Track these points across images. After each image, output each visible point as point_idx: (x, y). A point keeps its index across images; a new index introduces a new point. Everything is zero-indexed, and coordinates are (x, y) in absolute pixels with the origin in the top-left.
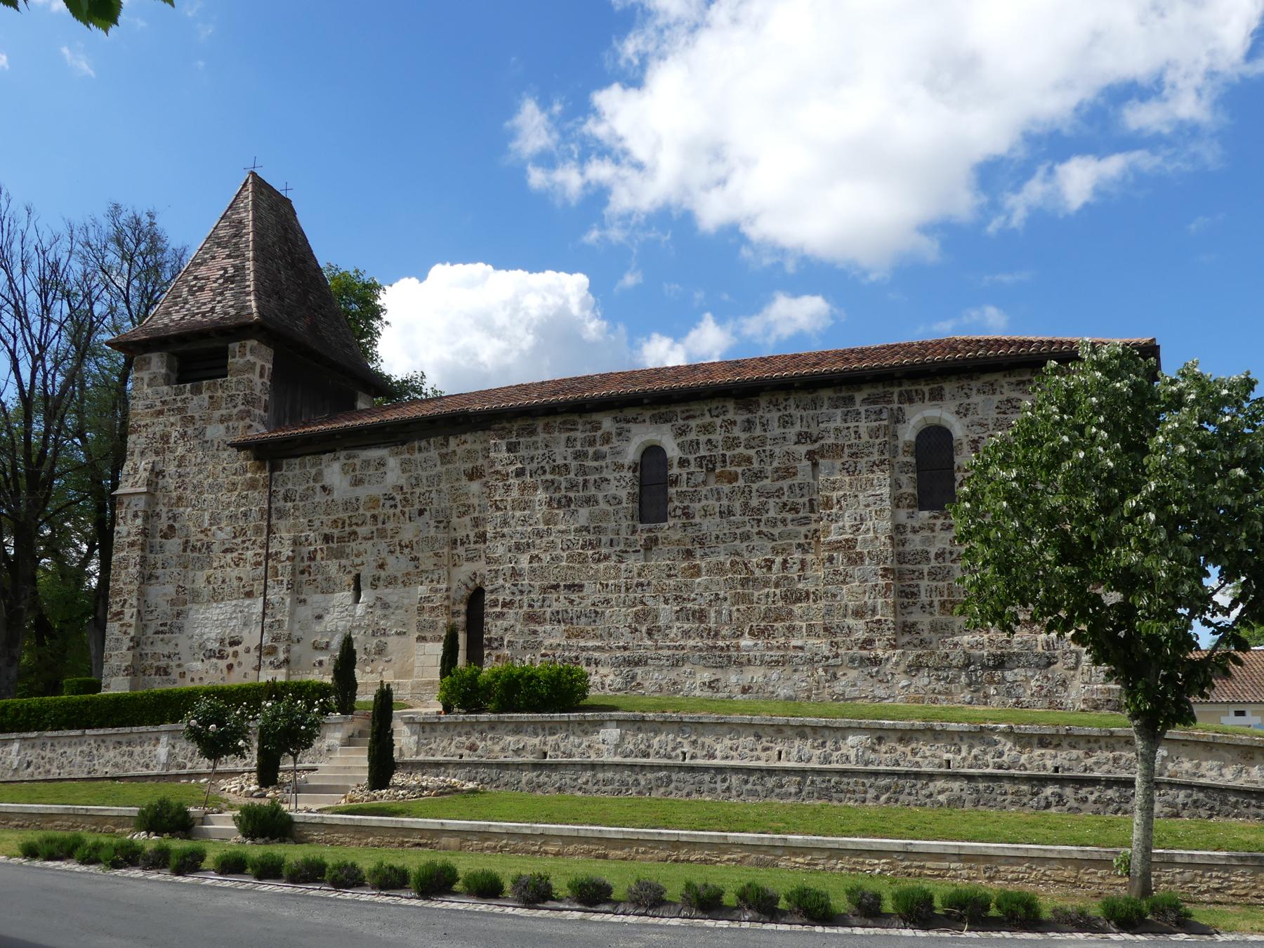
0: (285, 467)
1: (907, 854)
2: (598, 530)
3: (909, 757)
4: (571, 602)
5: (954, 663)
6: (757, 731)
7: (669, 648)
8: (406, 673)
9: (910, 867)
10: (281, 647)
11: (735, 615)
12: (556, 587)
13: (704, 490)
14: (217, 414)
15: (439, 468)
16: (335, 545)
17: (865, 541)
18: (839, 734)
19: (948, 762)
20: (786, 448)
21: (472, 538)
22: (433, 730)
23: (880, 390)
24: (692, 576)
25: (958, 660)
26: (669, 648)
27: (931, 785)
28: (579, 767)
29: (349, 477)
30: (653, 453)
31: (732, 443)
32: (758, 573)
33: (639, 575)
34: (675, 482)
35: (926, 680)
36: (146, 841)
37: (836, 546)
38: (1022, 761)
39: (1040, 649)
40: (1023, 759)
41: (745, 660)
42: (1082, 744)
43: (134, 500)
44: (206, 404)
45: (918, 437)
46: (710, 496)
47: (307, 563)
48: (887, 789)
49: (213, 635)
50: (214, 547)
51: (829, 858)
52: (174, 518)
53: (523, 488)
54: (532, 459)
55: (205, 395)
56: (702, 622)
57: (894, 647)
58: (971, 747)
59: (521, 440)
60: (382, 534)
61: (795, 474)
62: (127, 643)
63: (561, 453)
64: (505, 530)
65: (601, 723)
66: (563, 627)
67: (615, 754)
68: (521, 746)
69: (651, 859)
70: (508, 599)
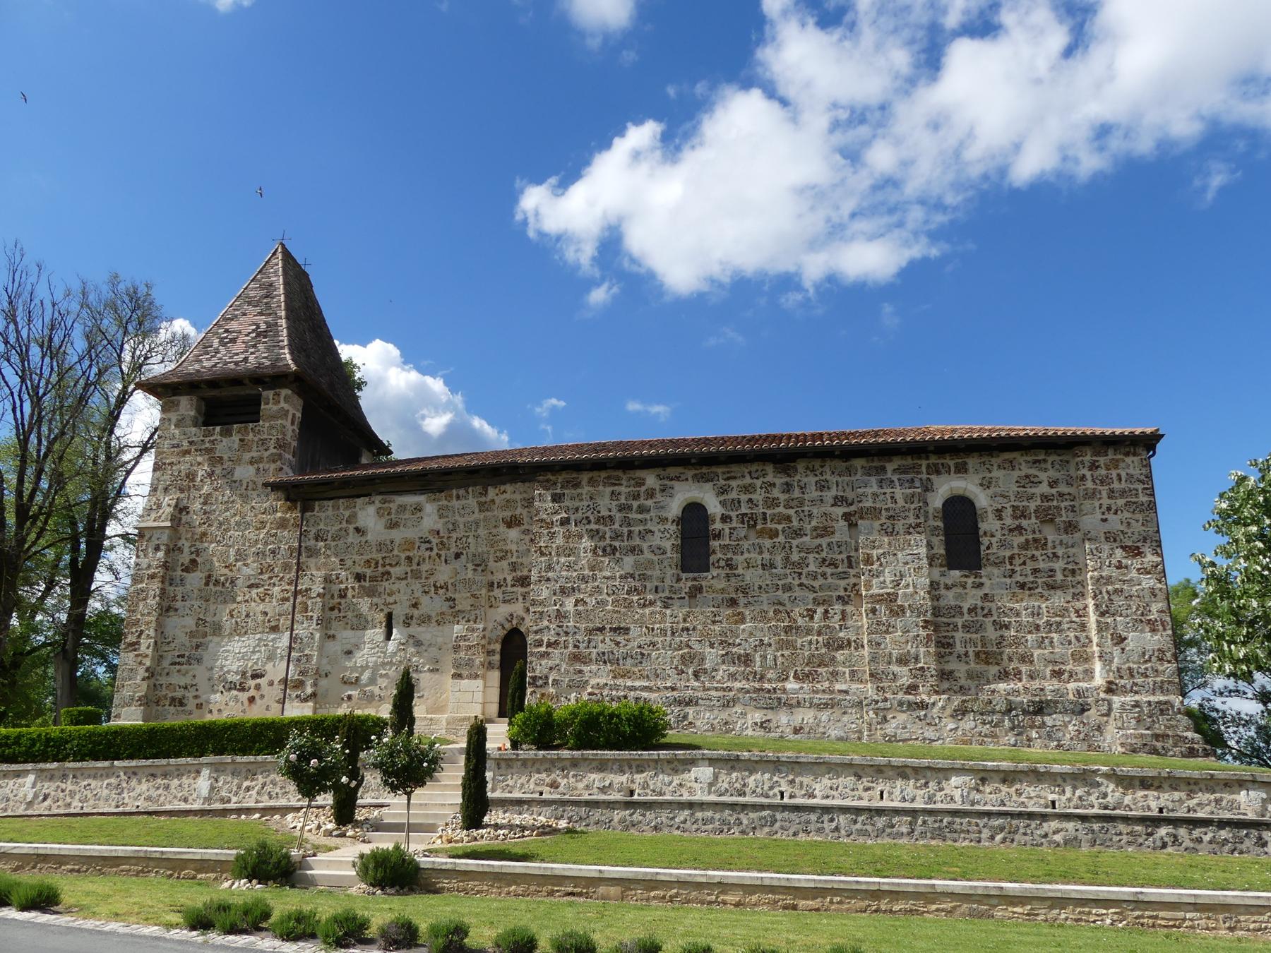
0: (317, 508)
1: (1138, 903)
2: (643, 577)
3: (1015, 798)
4: (618, 644)
5: (997, 708)
6: (858, 771)
7: (716, 689)
8: (439, 709)
9: (1142, 917)
10: (309, 683)
11: (780, 660)
12: (602, 629)
13: (746, 544)
14: (247, 456)
15: (476, 515)
16: (367, 584)
17: (905, 595)
18: (941, 775)
19: (1053, 803)
20: (823, 509)
21: (509, 582)
22: (509, 766)
23: (909, 461)
24: (736, 623)
25: (1001, 706)
26: (716, 689)
27: (1045, 825)
28: (675, 806)
29: (383, 521)
30: (694, 512)
31: (773, 503)
32: (800, 621)
33: (685, 620)
34: (718, 536)
35: (973, 724)
36: (240, 890)
37: (878, 599)
38: (1126, 802)
39: (1071, 697)
40: (1128, 800)
41: (794, 702)
42: (1183, 786)
43: (156, 534)
44: (236, 446)
45: (944, 505)
46: (752, 549)
47: (337, 600)
48: (1002, 829)
49: (234, 668)
50: (240, 582)
51: (1051, 908)
52: (198, 552)
53: (568, 537)
54: (577, 509)
55: (236, 438)
56: (748, 666)
57: (937, 693)
58: (1075, 788)
59: (566, 491)
60: (417, 575)
61: (833, 533)
62: (142, 673)
63: (606, 505)
64: (550, 574)
65: (693, 762)
66: (609, 667)
67: (710, 793)
68: (607, 784)
69: (848, 910)
70: (553, 639)
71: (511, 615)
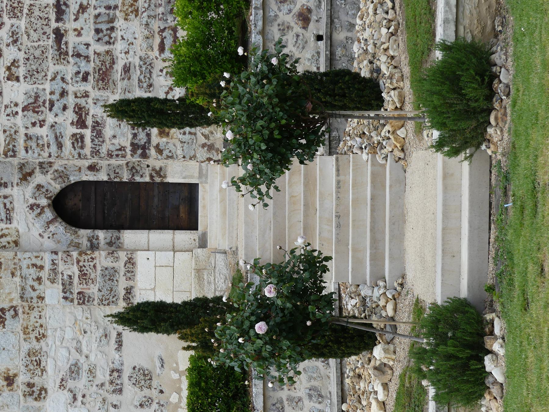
12: (59, 35)
66: (120, 23)
71: (32, 207)
